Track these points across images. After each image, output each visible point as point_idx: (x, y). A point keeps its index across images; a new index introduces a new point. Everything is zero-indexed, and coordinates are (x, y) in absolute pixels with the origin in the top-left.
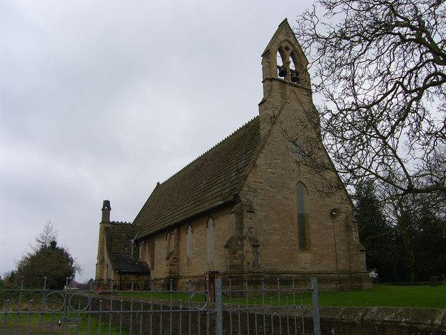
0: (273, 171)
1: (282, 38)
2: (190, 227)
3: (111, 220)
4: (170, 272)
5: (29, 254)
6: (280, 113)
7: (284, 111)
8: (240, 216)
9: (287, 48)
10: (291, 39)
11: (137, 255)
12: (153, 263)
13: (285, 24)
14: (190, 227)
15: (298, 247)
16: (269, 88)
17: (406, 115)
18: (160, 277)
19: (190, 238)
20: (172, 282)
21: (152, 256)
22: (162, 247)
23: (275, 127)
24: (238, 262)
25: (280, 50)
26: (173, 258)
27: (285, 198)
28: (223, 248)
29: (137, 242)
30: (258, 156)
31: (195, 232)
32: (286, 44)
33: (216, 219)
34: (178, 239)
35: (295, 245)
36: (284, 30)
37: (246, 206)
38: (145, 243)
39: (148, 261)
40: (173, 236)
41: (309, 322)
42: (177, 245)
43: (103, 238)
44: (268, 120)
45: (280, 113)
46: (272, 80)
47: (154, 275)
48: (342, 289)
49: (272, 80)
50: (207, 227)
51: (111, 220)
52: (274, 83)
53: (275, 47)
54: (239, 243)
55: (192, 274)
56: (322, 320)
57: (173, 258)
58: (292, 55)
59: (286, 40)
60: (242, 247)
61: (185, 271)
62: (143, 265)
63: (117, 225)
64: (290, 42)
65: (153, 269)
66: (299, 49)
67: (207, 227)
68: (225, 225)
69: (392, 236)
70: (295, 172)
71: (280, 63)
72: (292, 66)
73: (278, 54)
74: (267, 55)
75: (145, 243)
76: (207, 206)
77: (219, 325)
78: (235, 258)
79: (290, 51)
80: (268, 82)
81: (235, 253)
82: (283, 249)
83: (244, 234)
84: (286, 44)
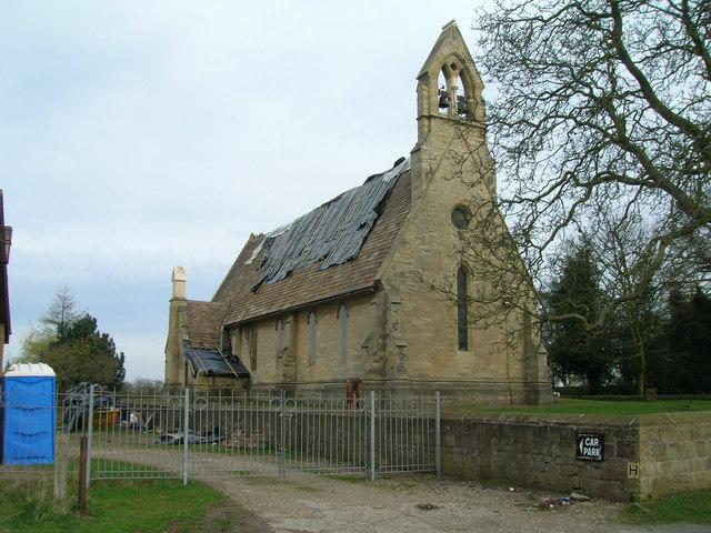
0: (427, 247)
1: (446, 50)
4: (284, 376)
5: (123, 356)
12: (254, 362)
13: (451, 32)
17: (565, 224)
18: (265, 381)
20: (287, 389)
21: (254, 353)
25: (444, 69)
26: (288, 355)
33: (351, 307)
34: (295, 330)
37: (501, 121)
41: (433, 421)
42: (295, 339)
46: (429, 117)
53: (436, 66)
55: (316, 379)
56: (441, 420)
57: (288, 355)
58: (461, 74)
61: (305, 373)
63: (562, 291)
65: (254, 369)
66: (471, 68)
68: (362, 319)
74: (424, 77)
75: (296, 321)
84: (453, 60)
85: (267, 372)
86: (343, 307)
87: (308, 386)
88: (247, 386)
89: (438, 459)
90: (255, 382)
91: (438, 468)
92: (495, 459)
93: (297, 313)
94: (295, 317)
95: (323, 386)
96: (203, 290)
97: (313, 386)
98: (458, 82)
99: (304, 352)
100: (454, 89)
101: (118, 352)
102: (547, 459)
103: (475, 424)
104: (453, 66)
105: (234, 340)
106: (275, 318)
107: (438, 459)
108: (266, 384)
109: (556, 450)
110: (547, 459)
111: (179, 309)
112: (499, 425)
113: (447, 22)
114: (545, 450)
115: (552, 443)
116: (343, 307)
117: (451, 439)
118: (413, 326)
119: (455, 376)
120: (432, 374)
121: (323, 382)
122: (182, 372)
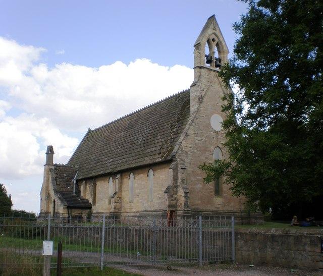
0: (199, 138)
2: (132, 174)
3: (54, 163)
4: (115, 208)
5: (10, 197)
6: (205, 95)
7: (209, 93)
8: (175, 170)
9: (213, 40)
10: (217, 32)
11: (78, 192)
14: (132, 174)
15: (213, 193)
16: (198, 74)
18: (102, 211)
19: (133, 183)
20: (115, 216)
22: (106, 188)
23: (202, 105)
24: (174, 202)
25: (208, 41)
26: (117, 196)
27: (206, 158)
28: (135, 181)
29: (78, 181)
30: (189, 128)
31: (136, 178)
32: (213, 36)
34: (121, 183)
35: (212, 192)
36: (212, 25)
38: (86, 183)
39: (90, 200)
40: (117, 180)
41: (231, 233)
42: (120, 188)
43: (48, 179)
44: (197, 100)
45: (205, 95)
46: (200, 68)
47: (95, 209)
48: (242, 224)
49: (200, 68)
50: (148, 176)
51: (54, 163)
52: (203, 70)
54: (175, 190)
57: (117, 196)
58: (217, 45)
59: (213, 33)
60: (176, 193)
62: (85, 201)
64: (215, 34)
65: (94, 203)
67: (148, 176)
69: (281, 23)
70: (214, 139)
71: (207, 52)
72: (216, 55)
73: (207, 44)
74: (197, 46)
75: (86, 183)
76: (147, 161)
77: (103, 245)
78: (172, 200)
79: (215, 43)
80: (198, 69)
81: (172, 196)
82: (203, 195)
83: (179, 184)
84: (213, 36)
85: (102, 206)
86: (151, 170)
87: (129, 214)
88: (90, 216)
89: (233, 254)
90: (94, 211)
91: (233, 258)
92: (269, 253)
93: (122, 172)
94: (121, 176)
95: (138, 214)
96: (64, 155)
97: (132, 214)
98: (215, 49)
99: (126, 195)
100: (214, 53)
101: (8, 194)
102: (303, 253)
103: (256, 235)
104: (213, 40)
105: (82, 188)
106: (112, 174)
107: (233, 254)
108: (102, 213)
109: (308, 248)
110: (303, 253)
111: (245, 146)
112: (271, 235)
113: (211, 15)
114: (301, 248)
115: (305, 244)
116: (151, 170)
117: (240, 243)
118: (192, 181)
119: (213, 208)
120: (201, 207)
121: (138, 212)
122: (52, 206)
